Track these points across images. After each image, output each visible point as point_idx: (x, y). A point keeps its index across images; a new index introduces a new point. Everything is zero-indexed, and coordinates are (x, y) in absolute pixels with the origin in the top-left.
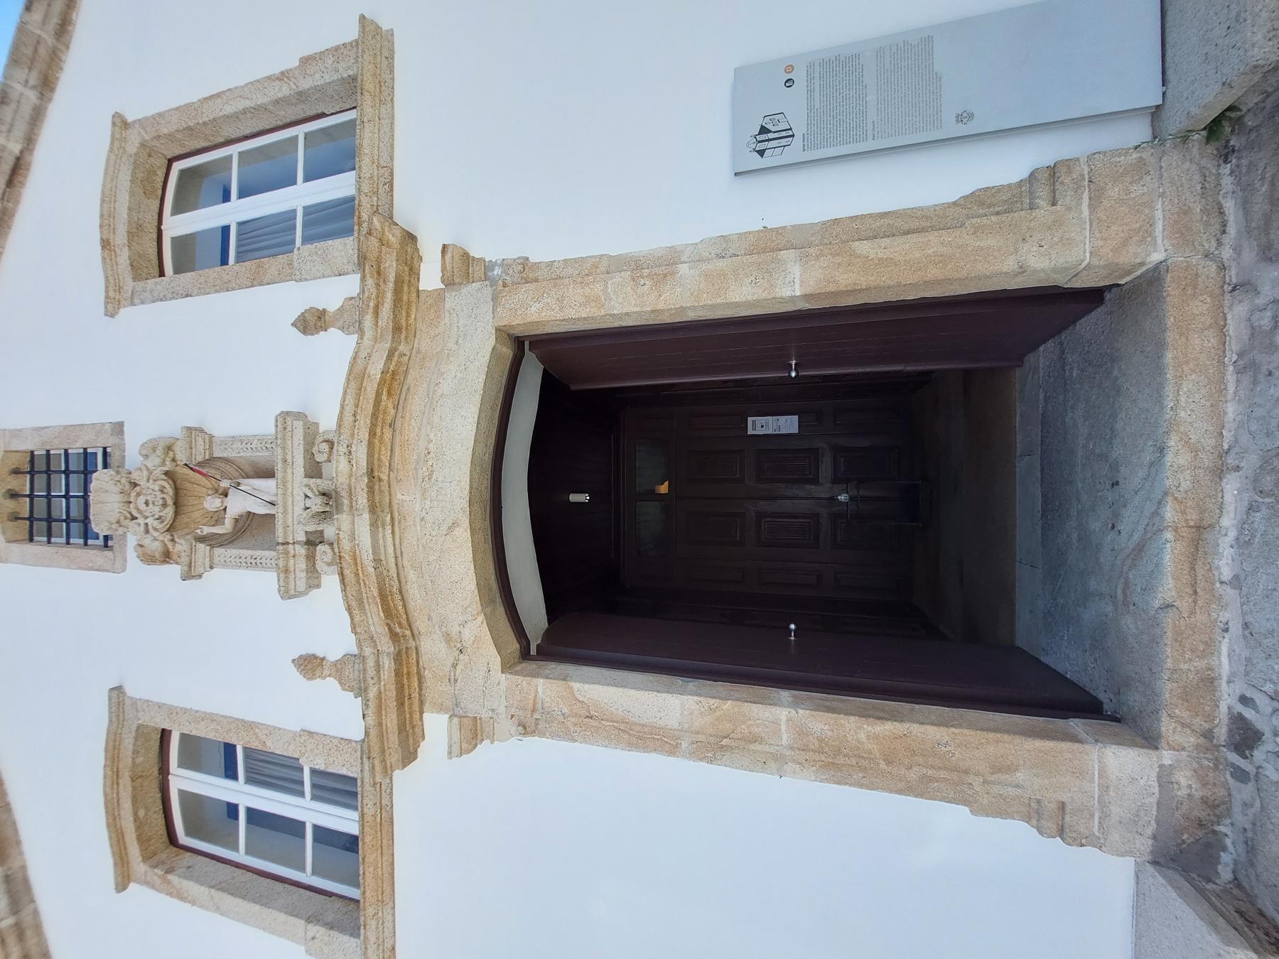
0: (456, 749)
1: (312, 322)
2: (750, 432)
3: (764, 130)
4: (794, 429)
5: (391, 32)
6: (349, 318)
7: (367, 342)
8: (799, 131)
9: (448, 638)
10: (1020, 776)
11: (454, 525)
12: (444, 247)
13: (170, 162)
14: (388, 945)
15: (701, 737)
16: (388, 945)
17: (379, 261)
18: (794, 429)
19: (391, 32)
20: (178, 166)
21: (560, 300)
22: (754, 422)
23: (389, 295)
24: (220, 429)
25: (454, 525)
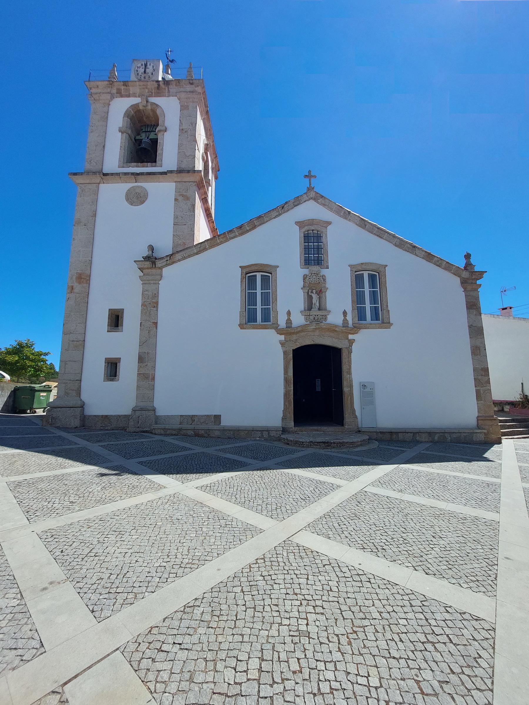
0: (280, 342)
1: (345, 313)
2: (317, 380)
3: (365, 386)
4: (317, 390)
5: (390, 328)
6: (345, 321)
7: (341, 328)
8: (364, 390)
9: (296, 340)
10: (289, 415)
11: (314, 341)
12: (354, 340)
13: (379, 273)
14: (246, 328)
15: (287, 378)
16: (246, 328)
17: (353, 330)
18: (317, 390)
19: (390, 328)
20: (377, 274)
21: (346, 358)
22: (319, 381)
23: (348, 331)
24: (328, 293)
25: (314, 341)
